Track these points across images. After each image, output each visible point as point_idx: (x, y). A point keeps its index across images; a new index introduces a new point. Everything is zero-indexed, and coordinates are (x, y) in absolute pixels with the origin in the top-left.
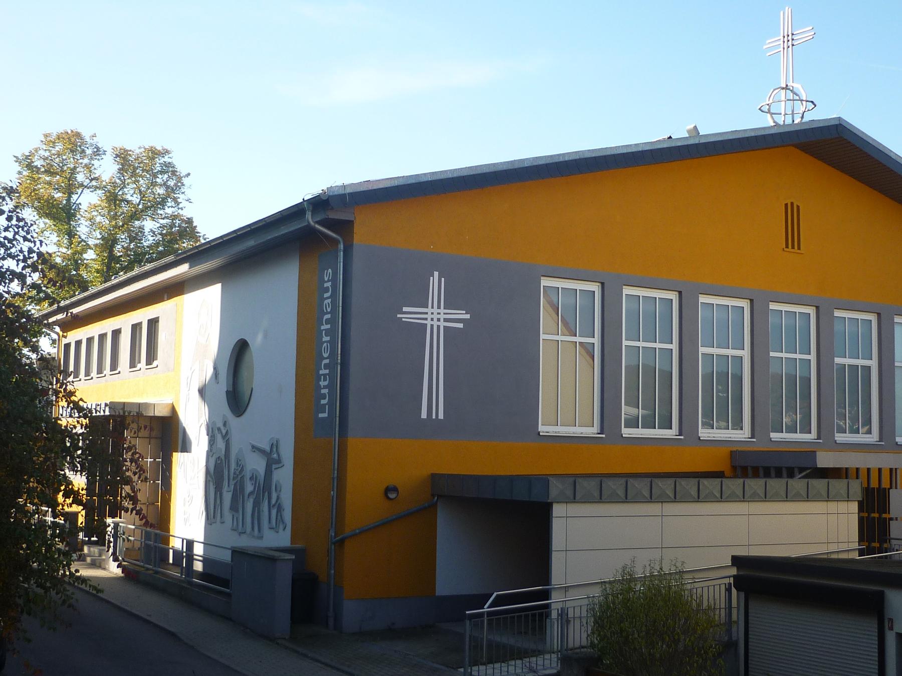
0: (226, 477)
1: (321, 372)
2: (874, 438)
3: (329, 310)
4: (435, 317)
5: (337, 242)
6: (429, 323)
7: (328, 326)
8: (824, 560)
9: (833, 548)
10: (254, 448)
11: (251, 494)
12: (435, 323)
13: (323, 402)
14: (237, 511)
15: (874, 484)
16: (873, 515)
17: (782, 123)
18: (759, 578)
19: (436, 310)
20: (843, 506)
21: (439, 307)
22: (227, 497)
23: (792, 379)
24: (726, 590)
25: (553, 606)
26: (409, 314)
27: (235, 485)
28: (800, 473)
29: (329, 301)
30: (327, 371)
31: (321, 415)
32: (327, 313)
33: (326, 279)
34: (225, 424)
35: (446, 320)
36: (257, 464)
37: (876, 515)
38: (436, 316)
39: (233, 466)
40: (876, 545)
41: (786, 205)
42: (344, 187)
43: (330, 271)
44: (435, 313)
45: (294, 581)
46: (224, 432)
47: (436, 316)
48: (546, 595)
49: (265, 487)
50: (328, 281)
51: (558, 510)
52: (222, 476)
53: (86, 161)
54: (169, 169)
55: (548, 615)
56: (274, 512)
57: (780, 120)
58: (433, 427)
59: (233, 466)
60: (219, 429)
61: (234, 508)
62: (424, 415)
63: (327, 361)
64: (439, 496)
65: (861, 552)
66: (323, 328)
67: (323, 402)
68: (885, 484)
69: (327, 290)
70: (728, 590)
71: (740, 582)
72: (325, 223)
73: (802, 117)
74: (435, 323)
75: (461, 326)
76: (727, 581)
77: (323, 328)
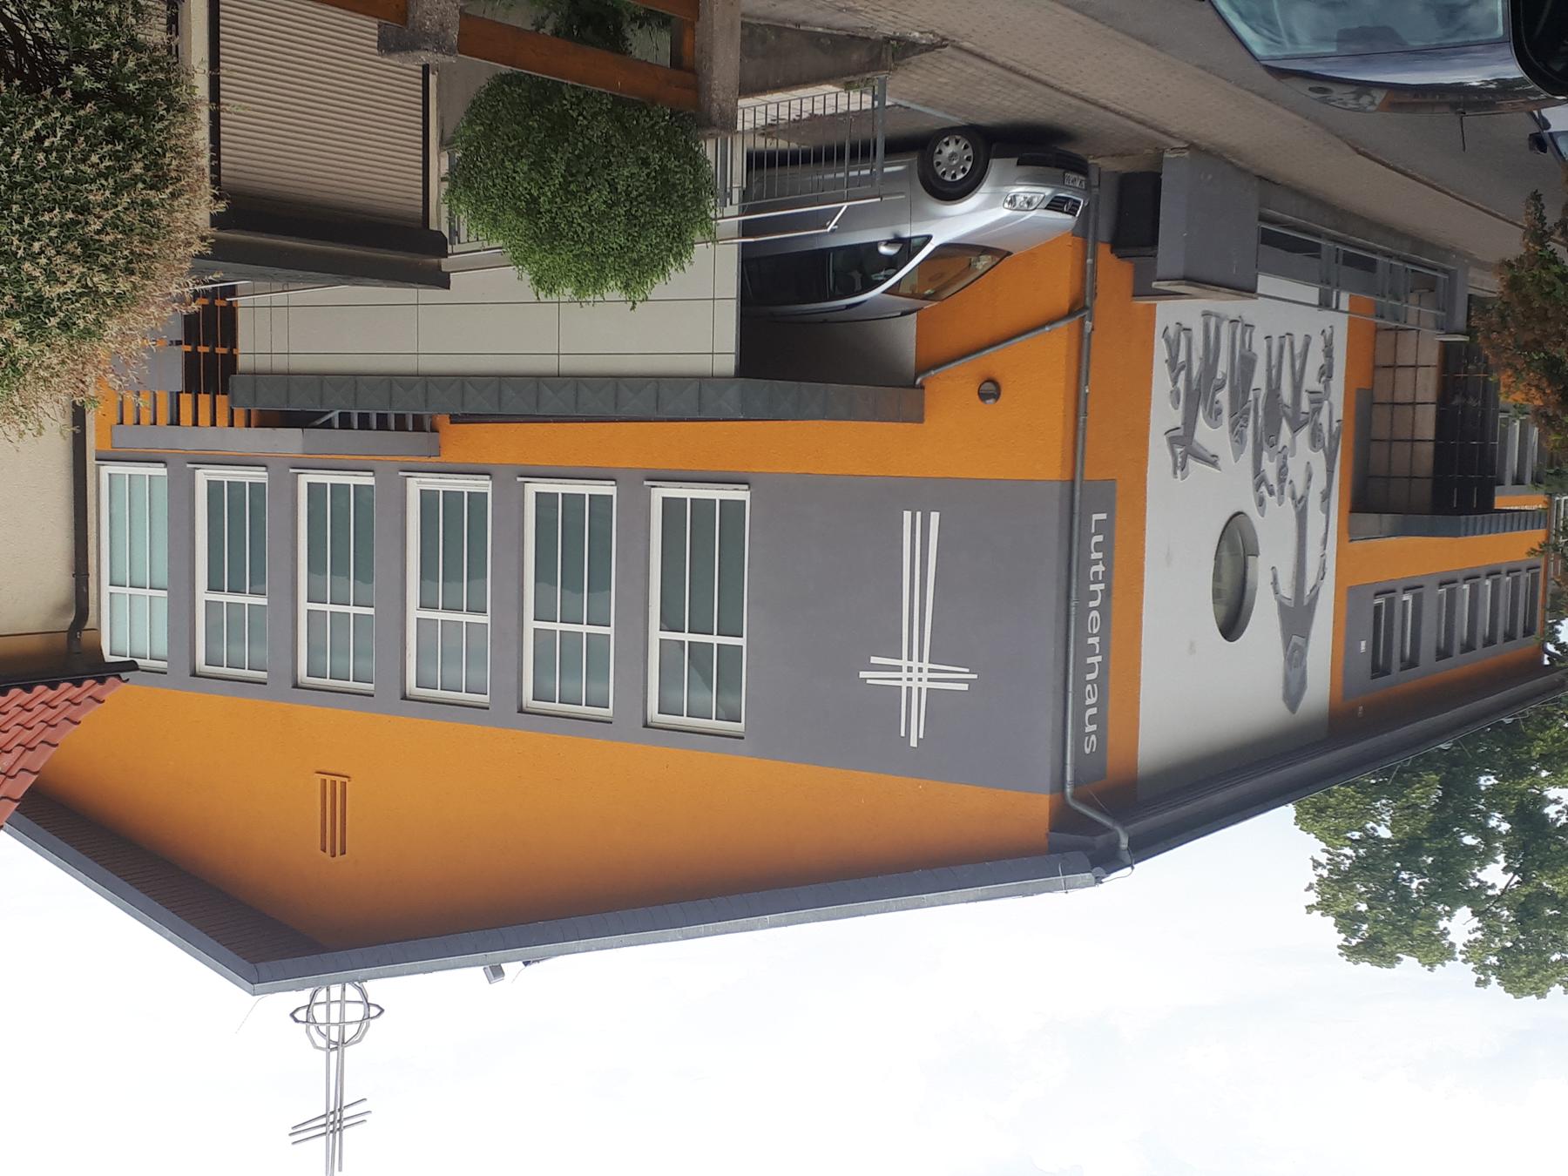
0: (1261, 413)
1: (1102, 586)
2: (203, 476)
3: (1089, 687)
4: (915, 675)
5: (1074, 797)
6: (926, 665)
7: (1090, 660)
8: (264, 277)
9: (279, 298)
10: (1212, 461)
11: (1220, 388)
12: (915, 664)
13: (1099, 538)
14: (1242, 357)
15: (205, 400)
16: (207, 349)
17: (348, 986)
18: (397, 248)
19: (915, 685)
20: (263, 363)
21: (909, 689)
22: (1259, 380)
23: (340, 569)
24: (457, 234)
25: (734, 210)
26: (957, 679)
27: (1246, 401)
28: (330, 420)
29: (1089, 702)
30: (1092, 587)
31: (1103, 516)
32: (1090, 682)
33: (1093, 738)
34: (1261, 502)
35: (899, 669)
36: (1212, 436)
37: (202, 349)
38: (914, 675)
39: (1249, 432)
40: (219, 303)
41: (343, 853)
42: (1067, 888)
43: (1087, 751)
44: (915, 679)
45: (1154, 241)
46: (1263, 488)
47: (914, 675)
48: (746, 229)
49: (1196, 398)
50: (1090, 734)
51: (728, 364)
52: (1266, 413)
53: (1497, 943)
54: (1348, 922)
55: (745, 195)
56: (1182, 358)
57: (352, 993)
58: (920, 493)
59: (1249, 432)
60: (1271, 493)
61: (1248, 363)
62: (935, 517)
63: (1092, 604)
64: (913, 386)
65: (232, 291)
66: (1099, 658)
67: (1099, 538)
68: (186, 401)
69: (1092, 719)
70: (454, 232)
71: (439, 245)
72: (1094, 828)
73: (313, 997)
74: (915, 664)
75: (874, 660)
76: (457, 248)
77: (1099, 658)
